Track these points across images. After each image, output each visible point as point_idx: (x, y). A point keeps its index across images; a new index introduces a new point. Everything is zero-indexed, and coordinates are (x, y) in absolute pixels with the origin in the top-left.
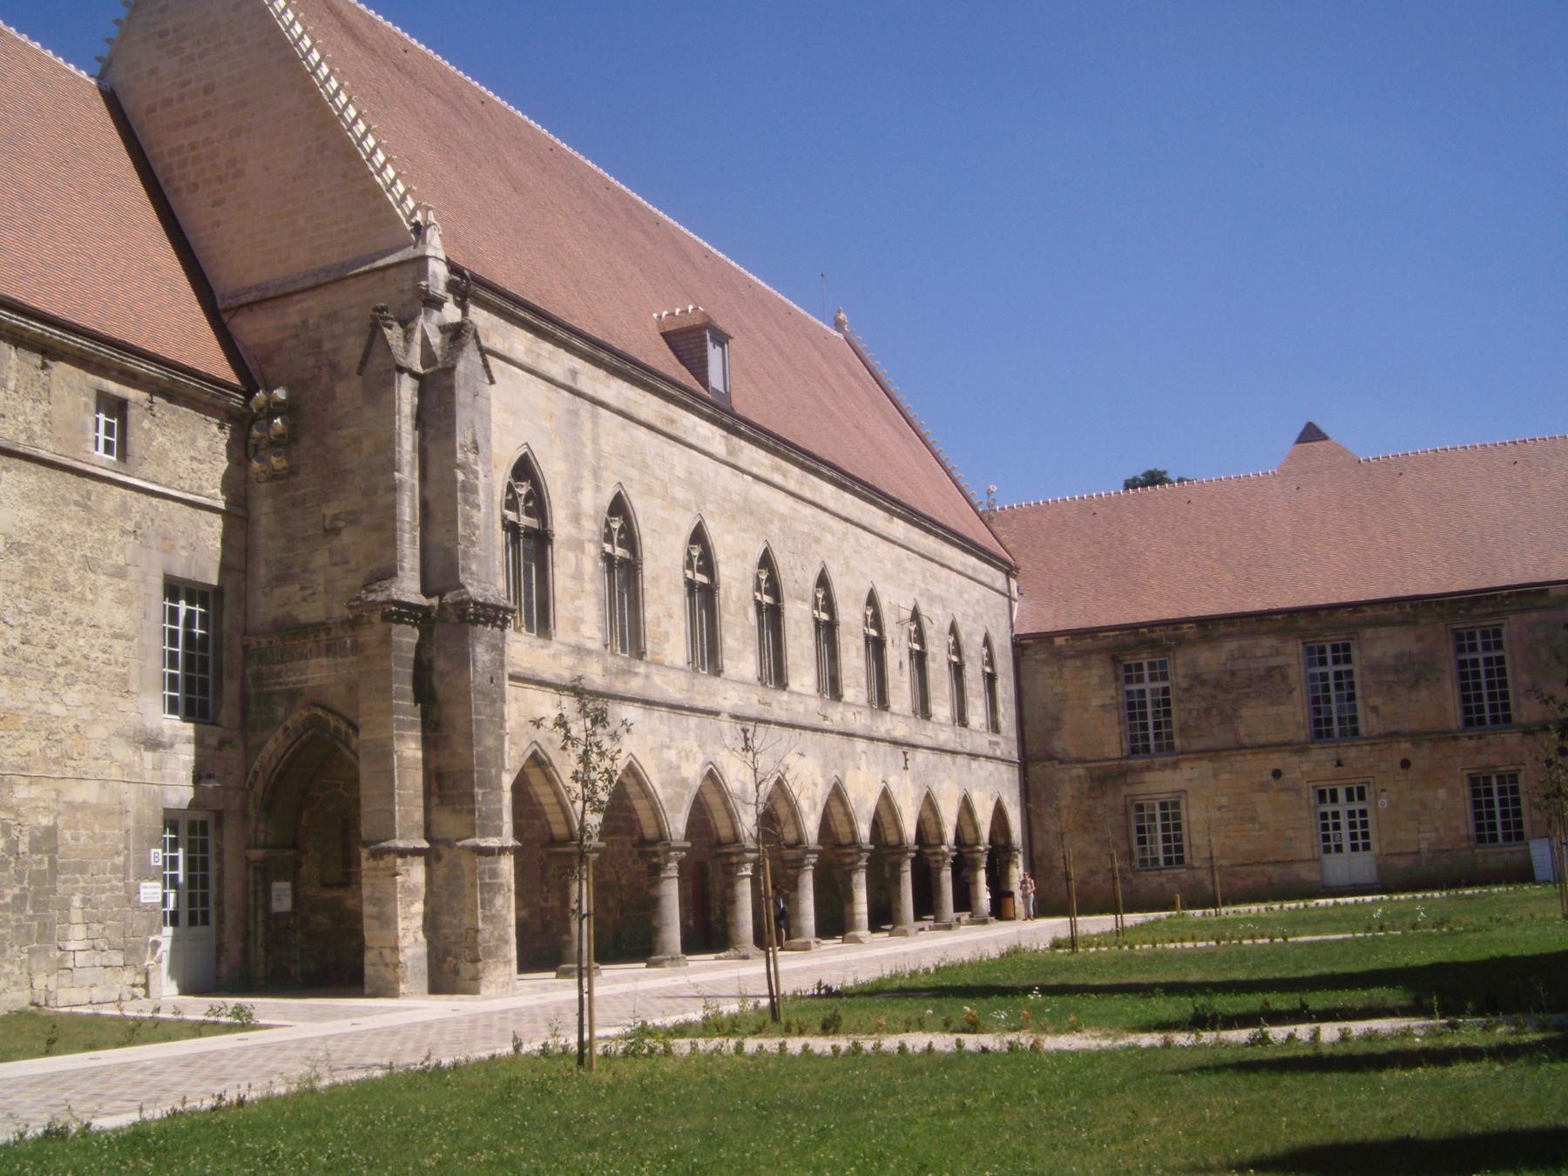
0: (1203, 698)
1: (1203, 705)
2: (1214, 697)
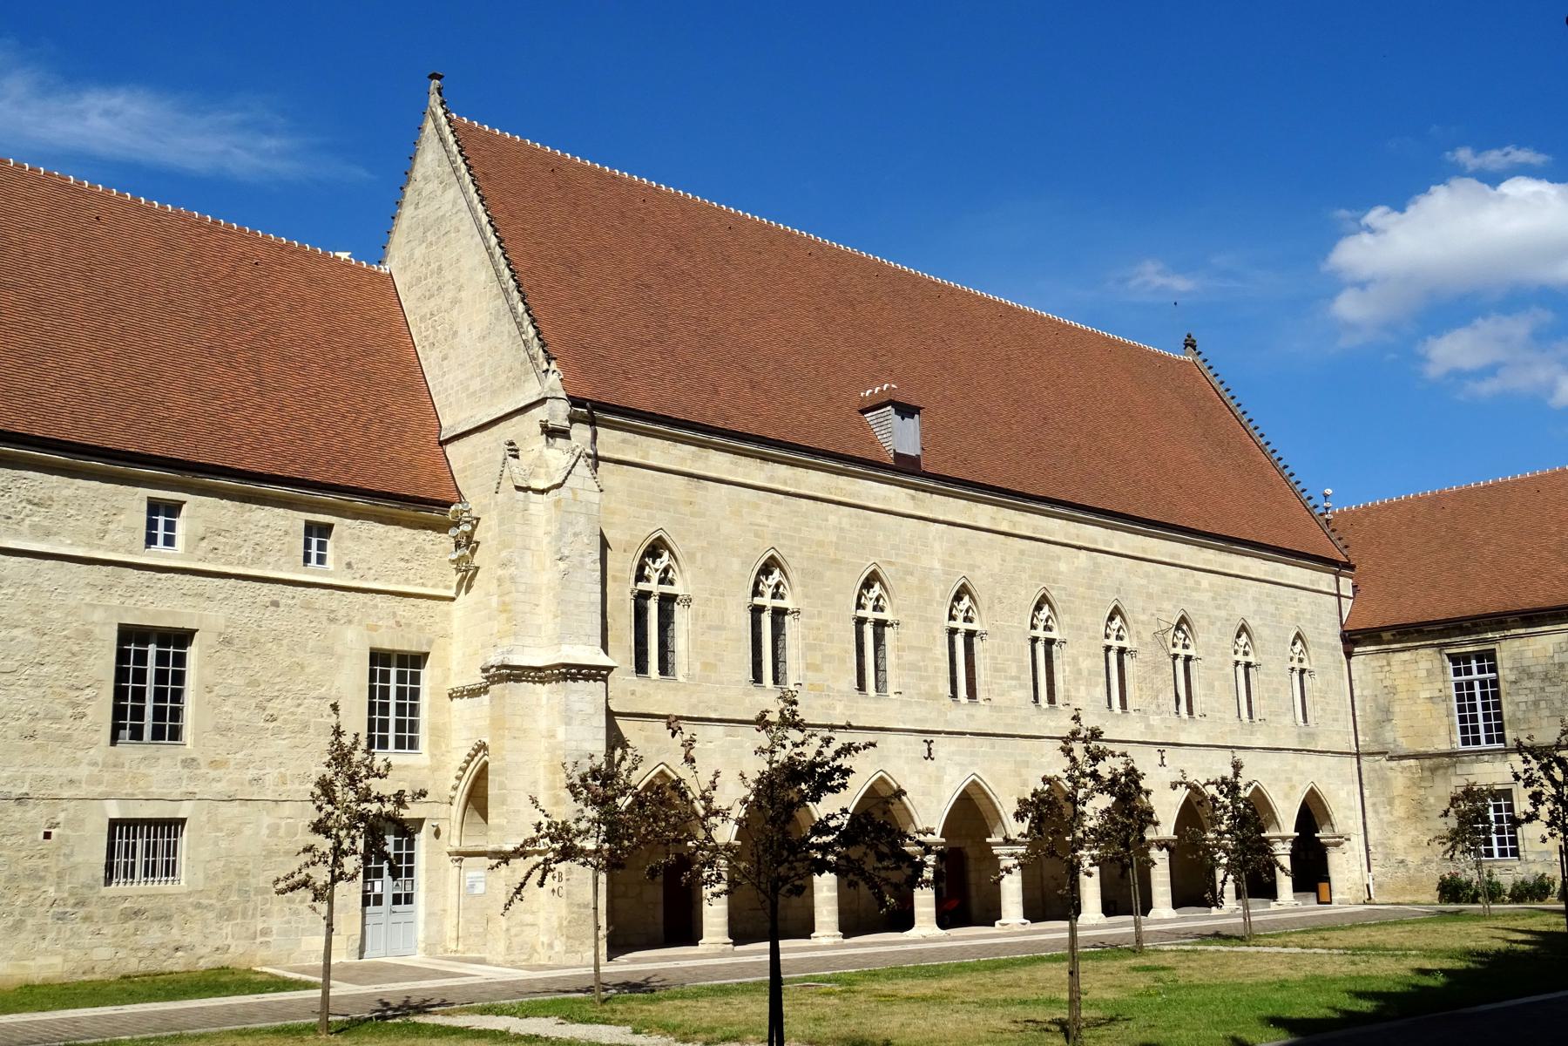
0: (1531, 690)
1: (1531, 697)
2: (1543, 689)
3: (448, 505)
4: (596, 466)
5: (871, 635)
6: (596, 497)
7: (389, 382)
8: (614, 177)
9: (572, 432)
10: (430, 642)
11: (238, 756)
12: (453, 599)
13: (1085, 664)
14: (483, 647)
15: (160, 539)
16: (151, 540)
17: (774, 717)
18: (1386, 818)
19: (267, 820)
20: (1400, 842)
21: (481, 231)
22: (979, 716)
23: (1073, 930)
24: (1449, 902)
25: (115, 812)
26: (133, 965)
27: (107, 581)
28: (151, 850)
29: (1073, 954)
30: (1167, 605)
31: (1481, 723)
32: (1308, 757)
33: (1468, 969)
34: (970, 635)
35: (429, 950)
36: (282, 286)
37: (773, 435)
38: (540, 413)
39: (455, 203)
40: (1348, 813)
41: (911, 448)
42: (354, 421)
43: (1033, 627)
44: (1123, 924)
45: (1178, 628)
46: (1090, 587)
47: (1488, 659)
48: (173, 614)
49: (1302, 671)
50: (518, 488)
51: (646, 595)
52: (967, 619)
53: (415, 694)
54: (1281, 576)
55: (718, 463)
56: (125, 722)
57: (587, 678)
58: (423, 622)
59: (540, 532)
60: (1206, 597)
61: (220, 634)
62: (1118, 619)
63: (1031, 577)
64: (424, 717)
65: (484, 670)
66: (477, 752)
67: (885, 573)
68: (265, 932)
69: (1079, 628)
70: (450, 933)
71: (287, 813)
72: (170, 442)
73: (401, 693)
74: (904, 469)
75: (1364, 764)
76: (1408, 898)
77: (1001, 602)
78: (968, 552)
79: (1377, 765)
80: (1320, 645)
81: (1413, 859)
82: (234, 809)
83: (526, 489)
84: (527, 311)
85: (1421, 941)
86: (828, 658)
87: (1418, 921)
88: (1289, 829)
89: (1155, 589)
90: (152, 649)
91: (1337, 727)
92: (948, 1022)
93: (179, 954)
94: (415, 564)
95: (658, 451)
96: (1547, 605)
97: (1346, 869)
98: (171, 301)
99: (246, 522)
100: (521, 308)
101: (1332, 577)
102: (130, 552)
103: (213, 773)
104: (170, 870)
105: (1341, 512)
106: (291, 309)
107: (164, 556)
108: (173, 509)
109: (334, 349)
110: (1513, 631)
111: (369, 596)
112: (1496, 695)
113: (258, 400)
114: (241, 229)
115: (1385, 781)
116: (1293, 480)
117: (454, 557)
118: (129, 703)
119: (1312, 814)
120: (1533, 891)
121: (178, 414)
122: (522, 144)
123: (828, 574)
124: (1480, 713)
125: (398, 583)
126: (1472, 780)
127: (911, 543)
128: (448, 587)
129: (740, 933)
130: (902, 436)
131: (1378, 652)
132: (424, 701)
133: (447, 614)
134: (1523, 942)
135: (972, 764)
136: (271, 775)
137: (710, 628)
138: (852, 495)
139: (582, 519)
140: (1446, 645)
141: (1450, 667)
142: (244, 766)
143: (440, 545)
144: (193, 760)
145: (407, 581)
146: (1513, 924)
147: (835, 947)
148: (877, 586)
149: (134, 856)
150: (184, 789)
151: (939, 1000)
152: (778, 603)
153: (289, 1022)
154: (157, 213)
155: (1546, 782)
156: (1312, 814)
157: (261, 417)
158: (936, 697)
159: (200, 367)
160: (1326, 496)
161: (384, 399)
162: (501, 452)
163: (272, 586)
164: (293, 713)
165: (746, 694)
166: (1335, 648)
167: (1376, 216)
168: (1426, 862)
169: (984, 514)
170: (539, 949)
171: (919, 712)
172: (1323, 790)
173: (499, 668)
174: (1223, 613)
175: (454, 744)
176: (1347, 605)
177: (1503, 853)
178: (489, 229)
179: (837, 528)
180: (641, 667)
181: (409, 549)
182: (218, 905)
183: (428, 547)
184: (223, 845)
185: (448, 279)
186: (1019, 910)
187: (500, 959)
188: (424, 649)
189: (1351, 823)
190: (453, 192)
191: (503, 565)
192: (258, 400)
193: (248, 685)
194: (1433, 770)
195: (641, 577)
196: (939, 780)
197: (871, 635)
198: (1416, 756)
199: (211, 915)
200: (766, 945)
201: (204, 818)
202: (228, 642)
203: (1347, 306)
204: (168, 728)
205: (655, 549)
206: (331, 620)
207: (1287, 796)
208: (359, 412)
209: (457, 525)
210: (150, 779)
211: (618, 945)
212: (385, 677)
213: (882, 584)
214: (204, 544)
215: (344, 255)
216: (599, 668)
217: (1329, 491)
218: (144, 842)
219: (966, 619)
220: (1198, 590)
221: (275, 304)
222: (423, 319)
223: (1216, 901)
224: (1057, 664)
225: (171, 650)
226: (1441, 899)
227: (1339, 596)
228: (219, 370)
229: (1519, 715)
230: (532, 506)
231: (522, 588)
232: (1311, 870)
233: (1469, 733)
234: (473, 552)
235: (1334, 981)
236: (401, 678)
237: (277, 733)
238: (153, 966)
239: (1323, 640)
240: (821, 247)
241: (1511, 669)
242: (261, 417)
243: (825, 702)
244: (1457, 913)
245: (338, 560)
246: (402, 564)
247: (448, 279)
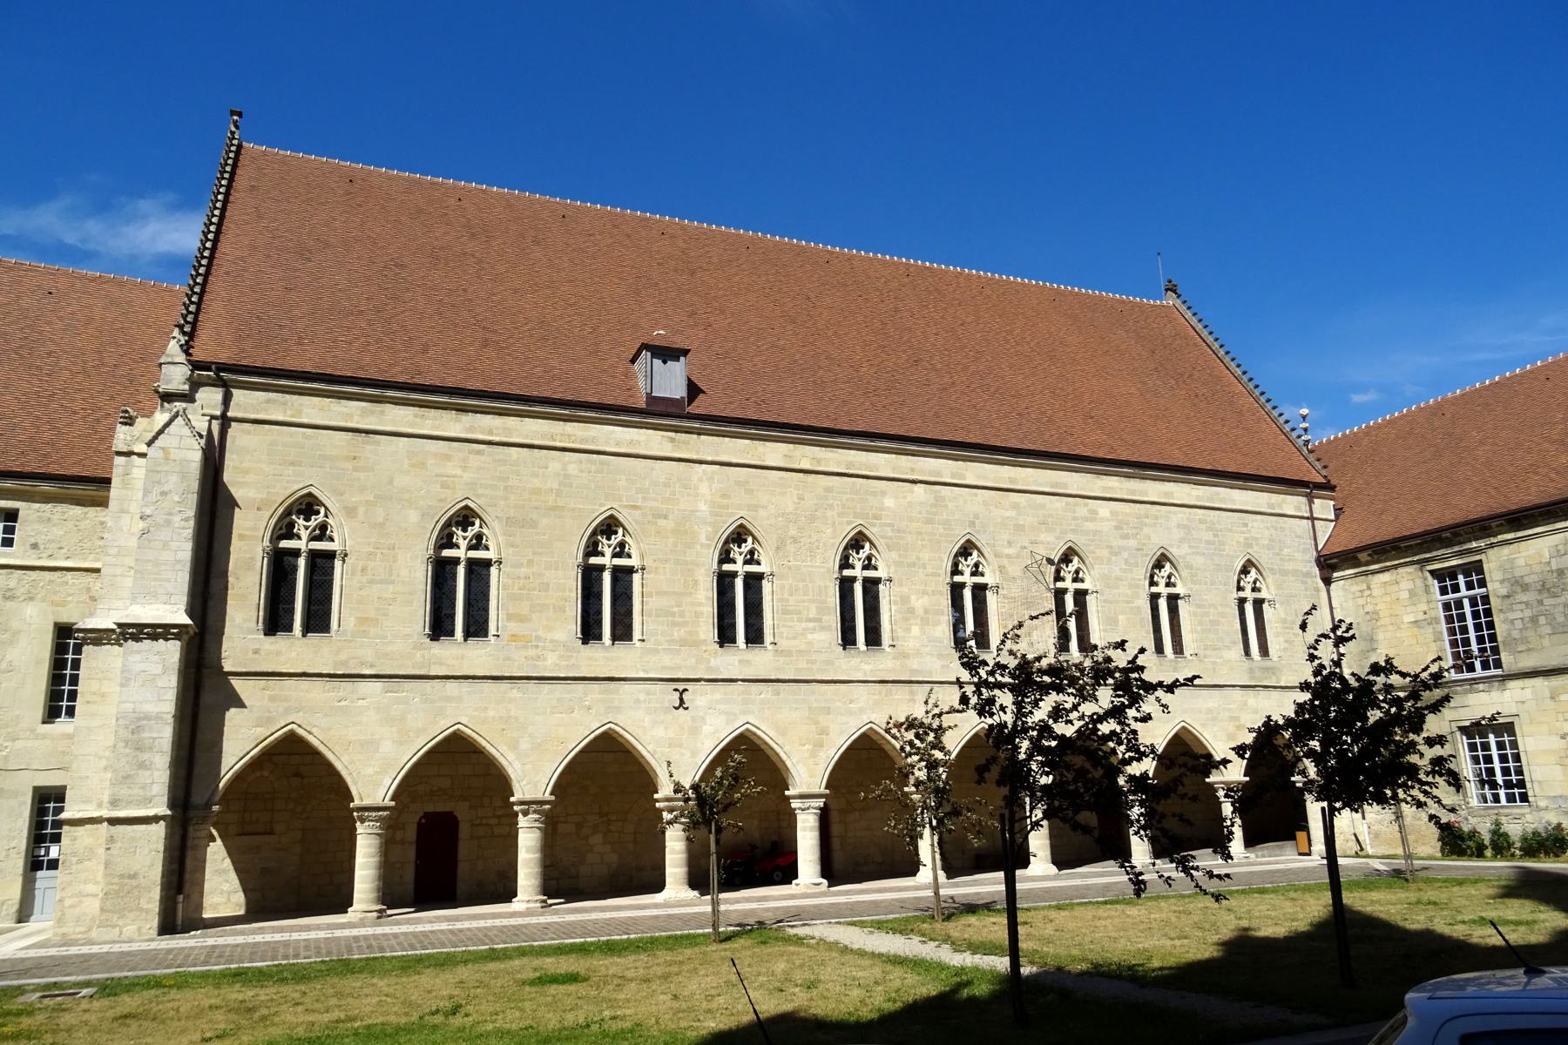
0: (1527, 603)
1: (1528, 613)
2: (1540, 602)
23: (1010, 882)
32: (1263, 693)
46: (929, 521)
51: (1063, 592)
54: (1065, 486)
63: (840, 515)
74: (658, 412)
101: (1304, 500)
110: (1500, 538)
111: (58, 574)
112: (1488, 613)
124: (1472, 635)
127: (666, 485)
130: (670, 381)
135: (744, 712)
139: (174, 478)
140: (1427, 561)
141: (1435, 585)
153: (116, 975)
160: (1304, 417)
166: (1308, 574)
171: (667, 660)
174: (1132, 543)
180: (1159, 649)
196: (695, 731)
200: (1001, 874)
217: (1305, 411)
219: (1168, 585)
220: (1093, 520)
223: (910, 867)
227: (1312, 519)
229: (1516, 634)
231: (114, 551)
239: (1290, 566)
241: (1502, 582)
243: (532, 652)
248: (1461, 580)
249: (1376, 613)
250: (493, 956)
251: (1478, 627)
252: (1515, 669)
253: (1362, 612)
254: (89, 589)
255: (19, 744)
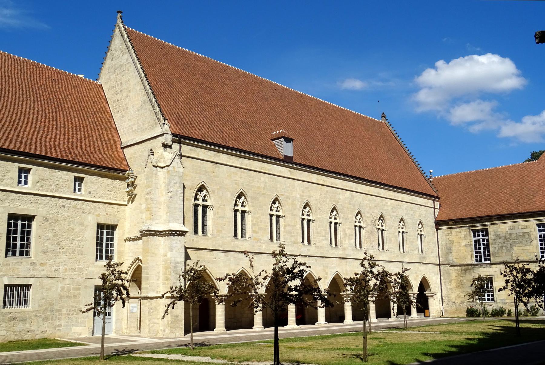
1: (500, 245)
2: (504, 243)
3: (125, 171)
4: (181, 158)
5: (240, 216)
6: (182, 170)
7: (102, 125)
8: (183, 51)
9: (173, 146)
10: (118, 221)
11: (50, 262)
12: (126, 205)
13: (348, 232)
14: (138, 223)
15: (23, 182)
16: (19, 182)
17: (277, 252)
18: (449, 287)
19: (60, 285)
20: (453, 296)
21: (138, 71)
22: (339, 252)
24: (470, 316)
25: (7, 281)
26: (13, 338)
27: (4, 197)
28: (19, 296)
29: (365, 332)
30: (376, 211)
31: (482, 254)
32: (423, 265)
33: (484, 338)
34: (309, 221)
35: (117, 333)
36: (63, 88)
37: (242, 148)
38: (162, 139)
39: (127, 60)
40: (436, 285)
41: (290, 153)
42: (91, 139)
43: (330, 218)
44: (360, 324)
45: (380, 219)
46: (350, 204)
47: (485, 231)
48: (28, 210)
49: (421, 235)
50: (154, 166)
52: (308, 215)
53: (112, 240)
54: (415, 201)
55: (223, 158)
56: (10, 249)
57: (178, 235)
58: (115, 213)
59: (161, 182)
60: (389, 208)
61: (44, 217)
62: (359, 215)
63: (330, 200)
64: (116, 248)
65: (140, 232)
66: (135, 261)
67: (281, 198)
68: (59, 326)
69: (346, 219)
70: (124, 326)
71: (67, 283)
72: (26, 146)
73: (107, 239)
74: (287, 161)
75: (442, 268)
76: (456, 315)
77: (319, 209)
78: (309, 191)
79: (446, 268)
80: (428, 226)
81: (458, 302)
82: (46, 281)
83: (156, 167)
84: (156, 101)
85: (465, 330)
86: (260, 229)
87: (462, 323)
88: (415, 290)
89: (372, 205)
90: (20, 222)
91: (433, 255)
92: (320, 356)
93: (29, 333)
94: (113, 192)
95: (202, 153)
96: (506, 213)
97: (434, 305)
98: (24, 94)
99: (53, 176)
100: (154, 100)
102: (12, 187)
103: (41, 268)
104: (25, 303)
105: (435, 178)
106: (67, 97)
107: (25, 188)
108: (28, 171)
109: (82, 113)
110: (494, 222)
111: (97, 204)
112: (488, 244)
113: (57, 131)
114: (47, 67)
115: (449, 274)
116: (419, 166)
117: (128, 190)
118: (11, 242)
119: (424, 285)
120: (499, 313)
121: (29, 136)
122: (150, 38)
123: (261, 198)
125: (107, 199)
126: (480, 274)
128: (125, 201)
129: (266, 325)
130: (286, 149)
131: (447, 228)
132: (116, 242)
133: (124, 211)
134: (499, 330)
136: (62, 269)
137: (220, 217)
138: (269, 170)
139: (177, 178)
141: (472, 234)
142: (52, 265)
143: (122, 186)
144: (34, 263)
145: (110, 198)
146: (493, 324)
147: (261, 331)
148: (277, 203)
149: (13, 298)
150: (31, 274)
151: (309, 348)
152: (243, 209)
154: (17, 60)
155: (510, 276)
156: (424, 285)
157: (58, 137)
158: (297, 243)
159: (36, 118)
160: (430, 172)
161: (101, 131)
162: (147, 153)
163: (62, 200)
164: (69, 246)
165: (232, 241)
166: (433, 227)
167: (440, 63)
168: (462, 303)
169: (314, 178)
170: (160, 332)
172: (427, 277)
173: (146, 231)
174: (395, 214)
175: (126, 258)
176: (437, 211)
177: (489, 300)
178: (141, 71)
179: (265, 182)
180: (196, 231)
181: (111, 187)
182: (43, 316)
183: (118, 186)
184: (45, 294)
185: (125, 89)
186: (324, 319)
187: (146, 335)
188: (116, 224)
189: (437, 289)
190: (127, 56)
191: (148, 194)
192: (57, 131)
193: (54, 236)
194: (466, 270)
195: (196, 199)
197: (240, 216)
198: (460, 265)
199: (40, 319)
200: (273, 328)
201: (38, 284)
202: (47, 220)
203: (423, 96)
204: (25, 252)
205: (201, 189)
206: (83, 213)
207: (415, 279)
208: (92, 136)
209: (128, 178)
210: (18, 270)
211: (187, 331)
212: (102, 233)
213: (279, 202)
214: (38, 184)
215: (81, 76)
216: (183, 231)
217: (431, 171)
218: (17, 292)
220: (387, 206)
221: (61, 95)
222: (114, 102)
224: (338, 231)
225: (26, 223)
226: (467, 316)
227: (434, 208)
228: (42, 120)
229: (496, 251)
230: (159, 173)
231: (155, 202)
232: (423, 305)
233: (478, 258)
234: (135, 188)
235: (441, 342)
236: (107, 234)
237: (64, 253)
238: (20, 338)
239: (429, 224)
240: (256, 78)
242: (58, 137)
243: (259, 244)
244: (474, 320)
245: (86, 190)
246: (109, 192)
247: (125, 89)
248: (481, 233)
249: (453, 241)
250: (323, 338)
251: (484, 248)
252: (494, 262)
253: (448, 240)
254: (106, 210)
255: (90, 269)
